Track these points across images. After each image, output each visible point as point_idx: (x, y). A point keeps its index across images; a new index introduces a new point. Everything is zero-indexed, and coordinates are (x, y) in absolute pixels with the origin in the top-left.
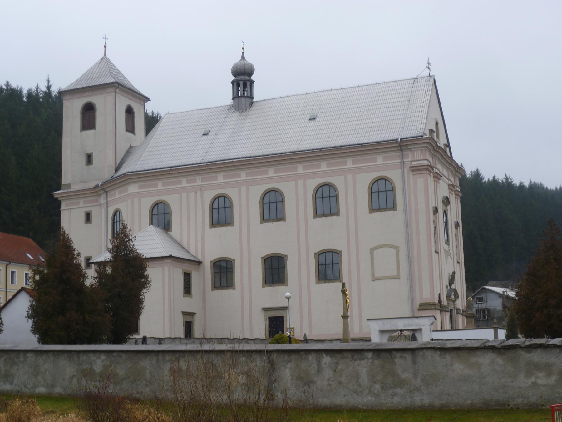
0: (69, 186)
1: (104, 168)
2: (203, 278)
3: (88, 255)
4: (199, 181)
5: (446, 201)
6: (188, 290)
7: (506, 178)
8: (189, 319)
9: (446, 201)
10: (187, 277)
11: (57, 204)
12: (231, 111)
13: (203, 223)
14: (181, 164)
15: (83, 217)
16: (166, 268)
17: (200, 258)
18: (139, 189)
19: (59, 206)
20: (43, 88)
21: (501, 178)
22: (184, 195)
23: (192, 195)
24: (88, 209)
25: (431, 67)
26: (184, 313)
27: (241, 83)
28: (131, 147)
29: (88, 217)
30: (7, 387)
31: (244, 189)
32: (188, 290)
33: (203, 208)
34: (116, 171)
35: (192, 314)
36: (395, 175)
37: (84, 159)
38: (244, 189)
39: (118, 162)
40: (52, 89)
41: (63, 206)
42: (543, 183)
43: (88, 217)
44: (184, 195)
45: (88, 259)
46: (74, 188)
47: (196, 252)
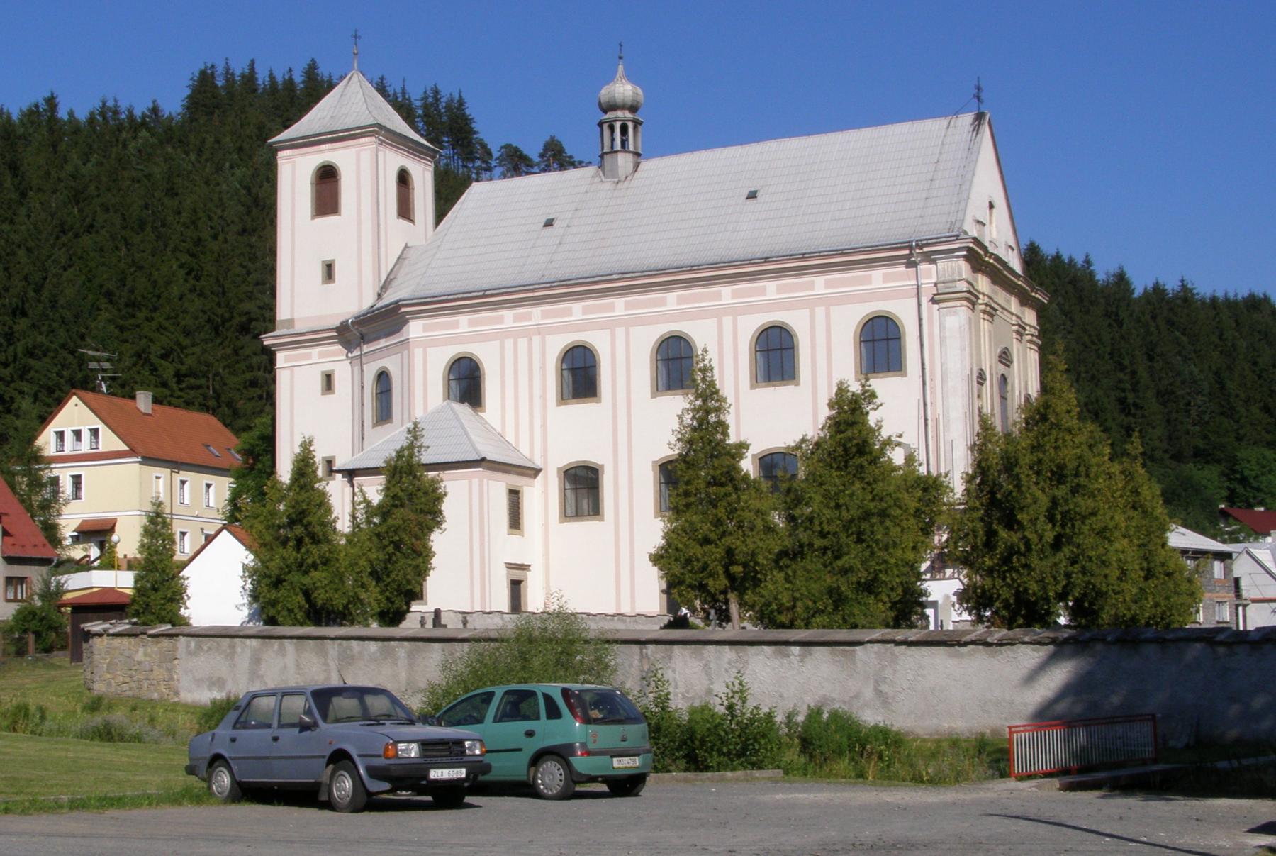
0: (291, 322)
1: (351, 298)
2: (542, 498)
3: (328, 454)
4: (536, 313)
5: (1005, 357)
6: (515, 522)
7: (1184, 287)
8: (517, 575)
9: (1005, 357)
10: (514, 495)
11: (270, 354)
12: (597, 179)
13: (544, 397)
14: (504, 284)
15: (318, 383)
16: (475, 481)
17: (538, 463)
18: (424, 331)
19: (272, 361)
20: (239, 68)
21: (1171, 285)
22: (509, 343)
23: (523, 343)
24: (327, 368)
25: (983, 95)
26: (511, 566)
27: (618, 125)
28: (406, 247)
29: (328, 380)
30: (1269, 453)
31: (620, 332)
32: (515, 522)
33: (543, 368)
34: (379, 296)
35: (524, 567)
36: (904, 312)
37: (319, 272)
38: (620, 332)
39: (383, 279)
40: (258, 68)
41: (281, 358)
42: (1268, 293)
43: (328, 380)
44: (509, 343)
45: (329, 462)
46: (299, 327)
47: (526, 452)
